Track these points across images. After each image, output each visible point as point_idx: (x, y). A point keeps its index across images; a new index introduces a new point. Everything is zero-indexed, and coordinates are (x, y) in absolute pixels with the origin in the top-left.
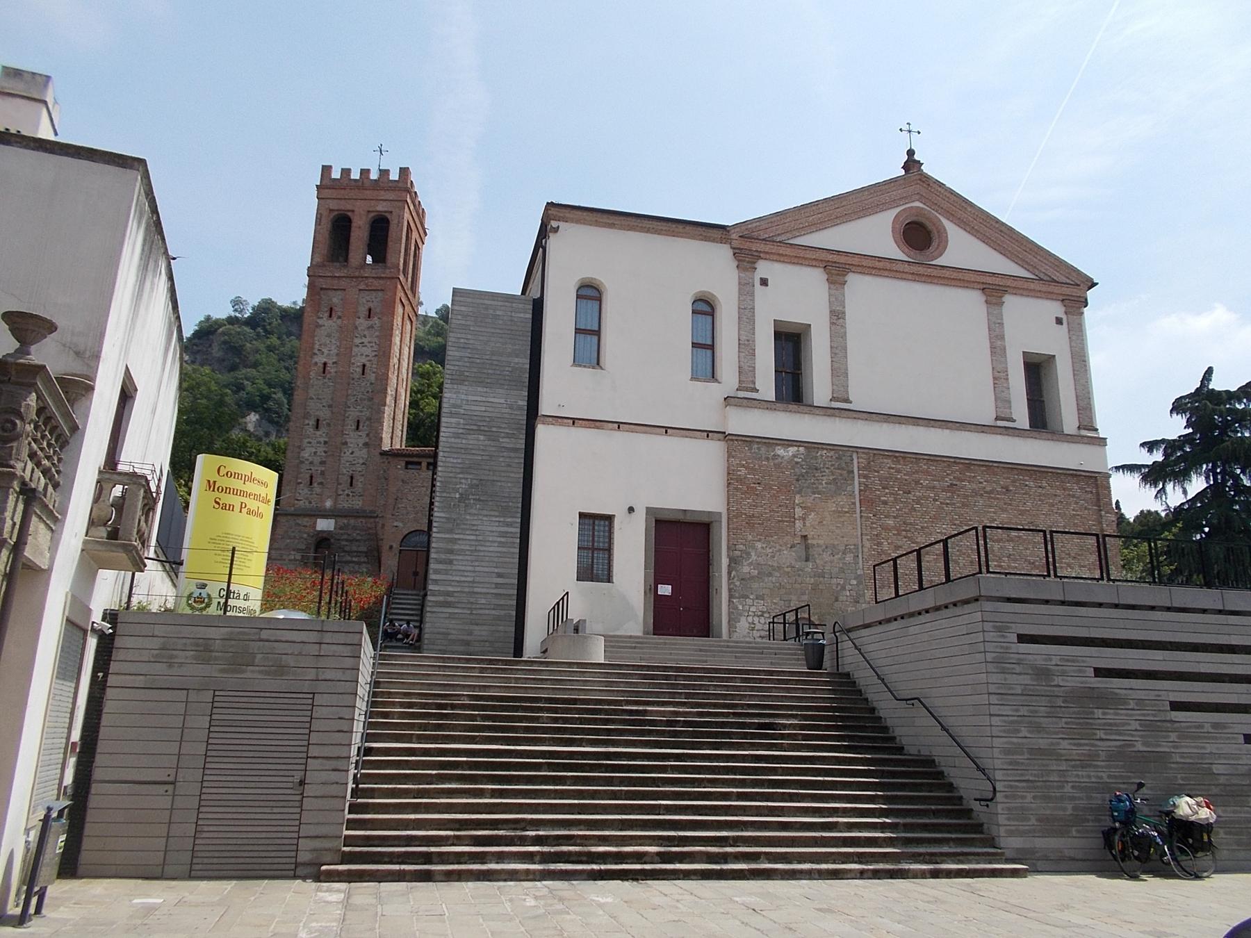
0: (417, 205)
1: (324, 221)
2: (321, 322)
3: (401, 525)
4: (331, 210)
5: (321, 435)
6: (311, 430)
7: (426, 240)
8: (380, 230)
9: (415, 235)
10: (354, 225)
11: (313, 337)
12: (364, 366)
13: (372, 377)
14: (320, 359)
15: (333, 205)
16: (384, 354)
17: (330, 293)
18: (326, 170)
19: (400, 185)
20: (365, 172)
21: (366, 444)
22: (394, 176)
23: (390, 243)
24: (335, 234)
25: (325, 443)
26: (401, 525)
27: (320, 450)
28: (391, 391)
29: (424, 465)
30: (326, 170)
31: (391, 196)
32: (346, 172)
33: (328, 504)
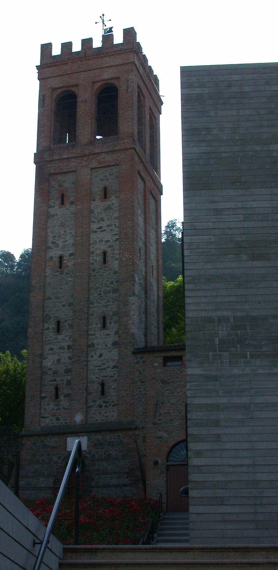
2: (52, 211)
3: (165, 435)
6: (51, 335)
8: (108, 97)
9: (148, 102)
10: (79, 99)
12: (105, 253)
13: (115, 265)
17: (60, 177)
18: (46, 48)
21: (115, 344)
22: (118, 39)
23: (120, 112)
25: (69, 347)
26: (165, 435)
27: (65, 356)
30: (46, 48)
31: (118, 60)
33: (79, 418)
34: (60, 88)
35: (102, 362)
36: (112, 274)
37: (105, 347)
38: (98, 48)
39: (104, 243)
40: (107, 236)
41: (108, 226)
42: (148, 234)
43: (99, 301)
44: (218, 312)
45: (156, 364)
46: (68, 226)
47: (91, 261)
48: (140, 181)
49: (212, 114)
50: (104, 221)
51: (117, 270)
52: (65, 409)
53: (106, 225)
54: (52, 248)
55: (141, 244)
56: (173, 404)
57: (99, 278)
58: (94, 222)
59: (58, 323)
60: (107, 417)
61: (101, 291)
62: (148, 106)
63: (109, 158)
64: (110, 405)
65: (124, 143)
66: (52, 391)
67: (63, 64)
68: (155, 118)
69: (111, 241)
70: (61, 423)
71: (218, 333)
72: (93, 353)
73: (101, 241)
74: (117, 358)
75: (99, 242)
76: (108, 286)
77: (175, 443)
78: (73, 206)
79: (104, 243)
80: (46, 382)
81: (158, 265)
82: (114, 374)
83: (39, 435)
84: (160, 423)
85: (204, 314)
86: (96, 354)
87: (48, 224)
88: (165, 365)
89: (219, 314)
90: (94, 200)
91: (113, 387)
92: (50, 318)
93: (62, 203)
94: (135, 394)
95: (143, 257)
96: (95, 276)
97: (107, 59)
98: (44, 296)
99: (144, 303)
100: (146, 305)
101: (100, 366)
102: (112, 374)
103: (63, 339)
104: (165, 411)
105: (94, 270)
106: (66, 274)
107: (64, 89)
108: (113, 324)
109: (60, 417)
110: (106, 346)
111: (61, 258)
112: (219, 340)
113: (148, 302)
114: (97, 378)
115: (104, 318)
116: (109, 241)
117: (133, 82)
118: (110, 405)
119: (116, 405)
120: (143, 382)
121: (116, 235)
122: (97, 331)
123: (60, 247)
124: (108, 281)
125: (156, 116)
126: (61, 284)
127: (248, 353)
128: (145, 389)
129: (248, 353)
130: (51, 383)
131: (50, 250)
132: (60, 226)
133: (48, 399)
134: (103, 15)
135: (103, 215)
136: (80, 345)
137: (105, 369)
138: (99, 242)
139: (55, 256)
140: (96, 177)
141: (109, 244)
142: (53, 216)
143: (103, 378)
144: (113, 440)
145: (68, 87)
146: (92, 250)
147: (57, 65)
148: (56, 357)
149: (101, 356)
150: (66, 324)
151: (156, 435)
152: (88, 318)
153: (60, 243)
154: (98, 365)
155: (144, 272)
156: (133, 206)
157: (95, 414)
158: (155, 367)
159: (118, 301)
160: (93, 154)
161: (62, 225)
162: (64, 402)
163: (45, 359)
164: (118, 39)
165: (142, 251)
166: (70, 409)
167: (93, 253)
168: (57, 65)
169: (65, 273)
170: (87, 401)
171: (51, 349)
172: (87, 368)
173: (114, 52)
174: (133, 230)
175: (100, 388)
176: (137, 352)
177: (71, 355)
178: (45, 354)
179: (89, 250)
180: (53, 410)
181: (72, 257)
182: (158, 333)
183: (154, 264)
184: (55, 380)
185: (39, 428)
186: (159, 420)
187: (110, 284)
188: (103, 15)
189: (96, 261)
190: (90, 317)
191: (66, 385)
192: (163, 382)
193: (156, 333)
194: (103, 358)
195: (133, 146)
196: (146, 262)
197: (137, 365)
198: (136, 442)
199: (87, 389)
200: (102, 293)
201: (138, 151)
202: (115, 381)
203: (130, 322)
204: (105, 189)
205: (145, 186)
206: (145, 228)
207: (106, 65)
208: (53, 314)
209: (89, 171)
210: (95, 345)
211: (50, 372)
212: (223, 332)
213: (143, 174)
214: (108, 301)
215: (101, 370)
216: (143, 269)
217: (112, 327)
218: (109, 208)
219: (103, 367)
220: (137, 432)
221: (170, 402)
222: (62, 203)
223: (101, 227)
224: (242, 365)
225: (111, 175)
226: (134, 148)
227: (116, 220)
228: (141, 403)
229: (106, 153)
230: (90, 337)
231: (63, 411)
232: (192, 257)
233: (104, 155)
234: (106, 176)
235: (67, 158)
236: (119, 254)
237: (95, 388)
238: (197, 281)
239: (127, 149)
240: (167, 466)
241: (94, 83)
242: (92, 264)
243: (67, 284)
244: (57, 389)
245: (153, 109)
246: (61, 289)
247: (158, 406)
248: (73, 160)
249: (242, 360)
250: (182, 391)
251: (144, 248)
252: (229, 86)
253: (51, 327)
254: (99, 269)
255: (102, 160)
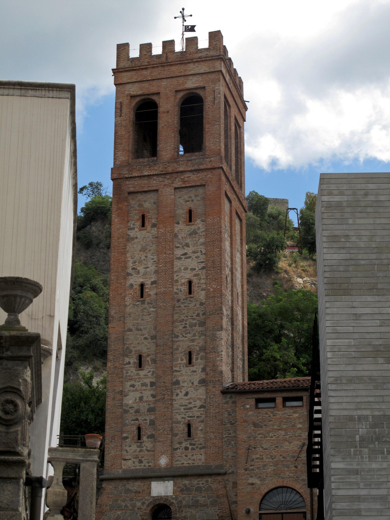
0: (233, 74)
1: (125, 110)
2: (132, 234)
3: (257, 481)
4: (133, 97)
5: (147, 374)
6: (132, 370)
7: (248, 114)
8: (192, 107)
9: (234, 111)
10: (161, 110)
11: (124, 253)
12: (190, 283)
13: (202, 295)
14: (135, 280)
15: (134, 90)
16: (213, 266)
17: (140, 197)
18: (122, 49)
19: (212, 53)
20: (168, 45)
21: (203, 382)
22: (203, 43)
23: (207, 127)
24: (141, 122)
25: (152, 384)
26: (257, 481)
27: (147, 394)
28: (226, 311)
29: (279, 401)
30: (122, 49)
31: (203, 68)
32: (146, 48)
33: (163, 461)
34: (140, 95)
35: (187, 401)
36: (198, 306)
37: (190, 384)
38: (181, 53)
39: (189, 271)
40: (193, 263)
41: (194, 252)
42: (234, 259)
43: (184, 334)
44: (358, 411)
45: (248, 406)
46: (150, 251)
47: (175, 290)
48: (226, 201)
49: (351, 221)
50: (189, 247)
51: (204, 301)
52: (148, 451)
53: (191, 251)
54: (132, 275)
55: (227, 271)
56: (267, 449)
57: (184, 309)
58: (178, 247)
59: (140, 357)
60: (194, 460)
61: (186, 324)
62: (234, 116)
63: (194, 178)
64: (197, 447)
65: (211, 161)
66: (134, 431)
67: (142, 69)
68: (240, 127)
69: (197, 269)
70: (145, 466)
71: (359, 431)
72: (178, 391)
73: (186, 269)
74: (204, 397)
75: (184, 270)
76: (194, 319)
77: (268, 490)
78: (155, 228)
79: (189, 271)
80: (127, 421)
81: (243, 292)
82: (201, 414)
83: (121, 479)
84: (253, 469)
85: (346, 413)
86: (181, 392)
87: (128, 248)
88: (257, 407)
89: (359, 413)
90: (178, 223)
91: (200, 428)
92: (131, 352)
93: (143, 225)
94: (224, 436)
95: (229, 286)
96: (180, 307)
97: (191, 66)
98: (124, 328)
99: (230, 335)
100: (232, 338)
101: (186, 405)
102: (199, 414)
103: (145, 375)
104: (258, 456)
105: (179, 301)
106: (148, 303)
107: (143, 97)
108: (199, 360)
109: (143, 459)
110: (193, 384)
111: (142, 286)
112: (359, 436)
113: (234, 334)
114: (183, 418)
115: (190, 353)
116: (195, 269)
117: (220, 93)
118: (197, 447)
119: (204, 447)
120: (232, 424)
121: (202, 262)
122: (182, 367)
123: (141, 274)
124: (194, 313)
125: (240, 124)
126: (143, 315)
127: (385, 449)
128: (235, 432)
129: (385, 449)
130: (133, 422)
131: (130, 277)
132: (140, 251)
133: (129, 439)
134: (183, 9)
135: (188, 241)
136: (164, 383)
137: (191, 408)
138: (184, 270)
139: (136, 283)
140: (179, 198)
141: (194, 272)
142: (133, 239)
143: (189, 419)
144: (201, 485)
145: (148, 95)
146: (175, 278)
147: (135, 70)
148: (138, 395)
149: (187, 394)
150: (148, 359)
151: (248, 482)
152: (172, 353)
153: (141, 269)
154: (184, 404)
155: (230, 302)
156: (221, 232)
157: (181, 456)
158: (247, 409)
159: (205, 335)
160: (177, 173)
161: (143, 249)
162: (147, 443)
163: (126, 396)
164: (203, 43)
165: (229, 279)
166: (154, 451)
167: (177, 281)
168: (135, 70)
169: (146, 303)
170: (172, 442)
171: (133, 386)
172: (172, 407)
173: (199, 58)
174: (221, 259)
175: (186, 430)
176: (225, 392)
177: (154, 393)
178: (126, 390)
179: (172, 279)
180: (135, 451)
181: (154, 285)
182: (243, 366)
183: (239, 290)
184: (137, 420)
185: (120, 471)
186: (251, 466)
187: (197, 316)
188: (183, 9)
189: (181, 291)
190: (175, 352)
191: (150, 425)
192: (255, 425)
193: (241, 366)
194: (189, 396)
195: (221, 165)
196: (232, 290)
197: (226, 405)
198: (225, 487)
199: (172, 430)
200: (187, 325)
201: (225, 170)
202: (202, 421)
203: (218, 359)
204: (190, 212)
205: (231, 206)
206: (232, 253)
207: (191, 73)
208: (134, 347)
209: (173, 191)
210: (181, 382)
211: (132, 411)
212: (363, 430)
213: (229, 194)
214: (194, 335)
215: (188, 409)
216: (230, 298)
217: (199, 363)
218: (194, 233)
219: (190, 406)
220: (226, 477)
221: (262, 447)
222: (143, 225)
223: (185, 254)
224: (380, 460)
225: (196, 196)
226: (222, 168)
227: (202, 247)
228: (231, 447)
229: (191, 171)
230: (175, 373)
231: (146, 452)
232: (334, 359)
233: (189, 174)
234: (190, 197)
235: (148, 176)
236: (206, 284)
237: (182, 428)
238: (339, 382)
239: (214, 169)
240: (260, 514)
241: (177, 91)
242: (176, 293)
243: (149, 315)
244: (139, 429)
245: (238, 118)
246: (142, 320)
247: (250, 451)
248: (155, 178)
249: (380, 456)
250: (275, 436)
251: (230, 276)
252: (366, 195)
253: (132, 362)
254: (184, 300)
255: (186, 179)
